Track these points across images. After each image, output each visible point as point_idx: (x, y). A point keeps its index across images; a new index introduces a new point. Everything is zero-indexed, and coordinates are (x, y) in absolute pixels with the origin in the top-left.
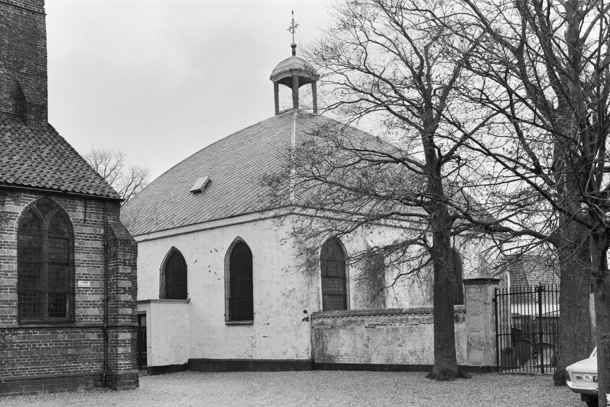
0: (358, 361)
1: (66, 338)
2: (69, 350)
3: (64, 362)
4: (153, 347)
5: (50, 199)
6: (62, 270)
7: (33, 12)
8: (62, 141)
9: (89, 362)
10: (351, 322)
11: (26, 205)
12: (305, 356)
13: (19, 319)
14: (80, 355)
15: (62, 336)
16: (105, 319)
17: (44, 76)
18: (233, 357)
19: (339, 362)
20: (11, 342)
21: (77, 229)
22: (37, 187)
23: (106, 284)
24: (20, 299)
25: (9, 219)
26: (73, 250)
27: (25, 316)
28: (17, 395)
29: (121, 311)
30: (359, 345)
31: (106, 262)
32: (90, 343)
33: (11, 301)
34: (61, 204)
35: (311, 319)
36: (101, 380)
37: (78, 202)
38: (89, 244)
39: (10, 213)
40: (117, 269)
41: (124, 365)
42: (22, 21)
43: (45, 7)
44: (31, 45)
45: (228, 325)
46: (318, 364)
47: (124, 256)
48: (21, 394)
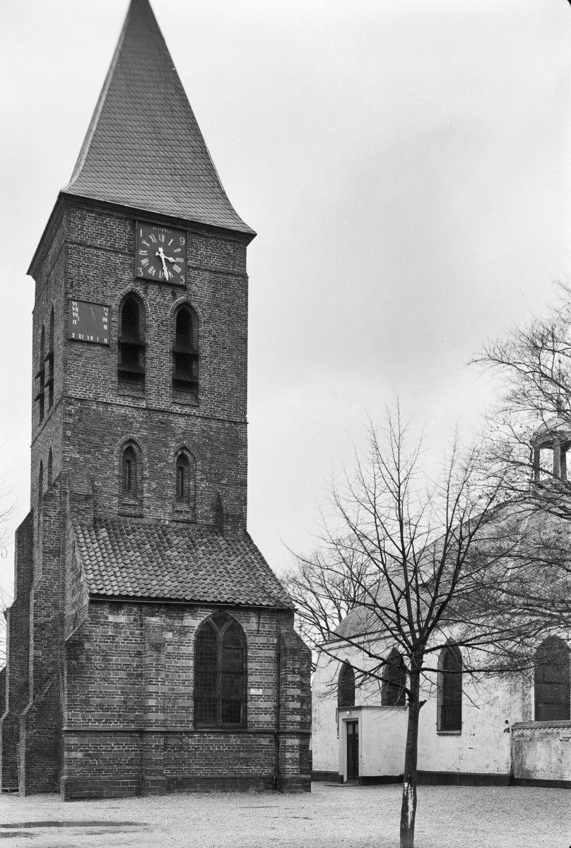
0: (552, 777)
1: (238, 743)
2: (241, 753)
3: (236, 764)
4: (364, 756)
5: (224, 611)
6: (237, 678)
7: (235, 423)
8: (255, 550)
9: (261, 766)
10: (548, 734)
11: (203, 619)
12: (505, 771)
13: (195, 722)
14: (251, 758)
15: (234, 740)
16: (277, 725)
17: (244, 484)
18: (443, 769)
19: (535, 778)
20: (188, 744)
21: (250, 640)
22: (213, 602)
23: (278, 692)
24: (196, 706)
25: (187, 632)
26: (246, 659)
27: (201, 721)
28: (192, 792)
29: (289, 718)
30: (554, 760)
31: (278, 671)
32: (262, 748)
33: (188, 707)
34: (235, 616)
35: (513, 730)
36: (272, 783)
37: (252, 614)
38: (262, 653)
39: (188, 627)
40: (286, 678)
41: (291, 770)
42: (225, 433)
43: (247, 416)
44: (232, 455)
45: (439, 734)
46: (514, 780)
47: (293, 665)
48: (196, 792)
